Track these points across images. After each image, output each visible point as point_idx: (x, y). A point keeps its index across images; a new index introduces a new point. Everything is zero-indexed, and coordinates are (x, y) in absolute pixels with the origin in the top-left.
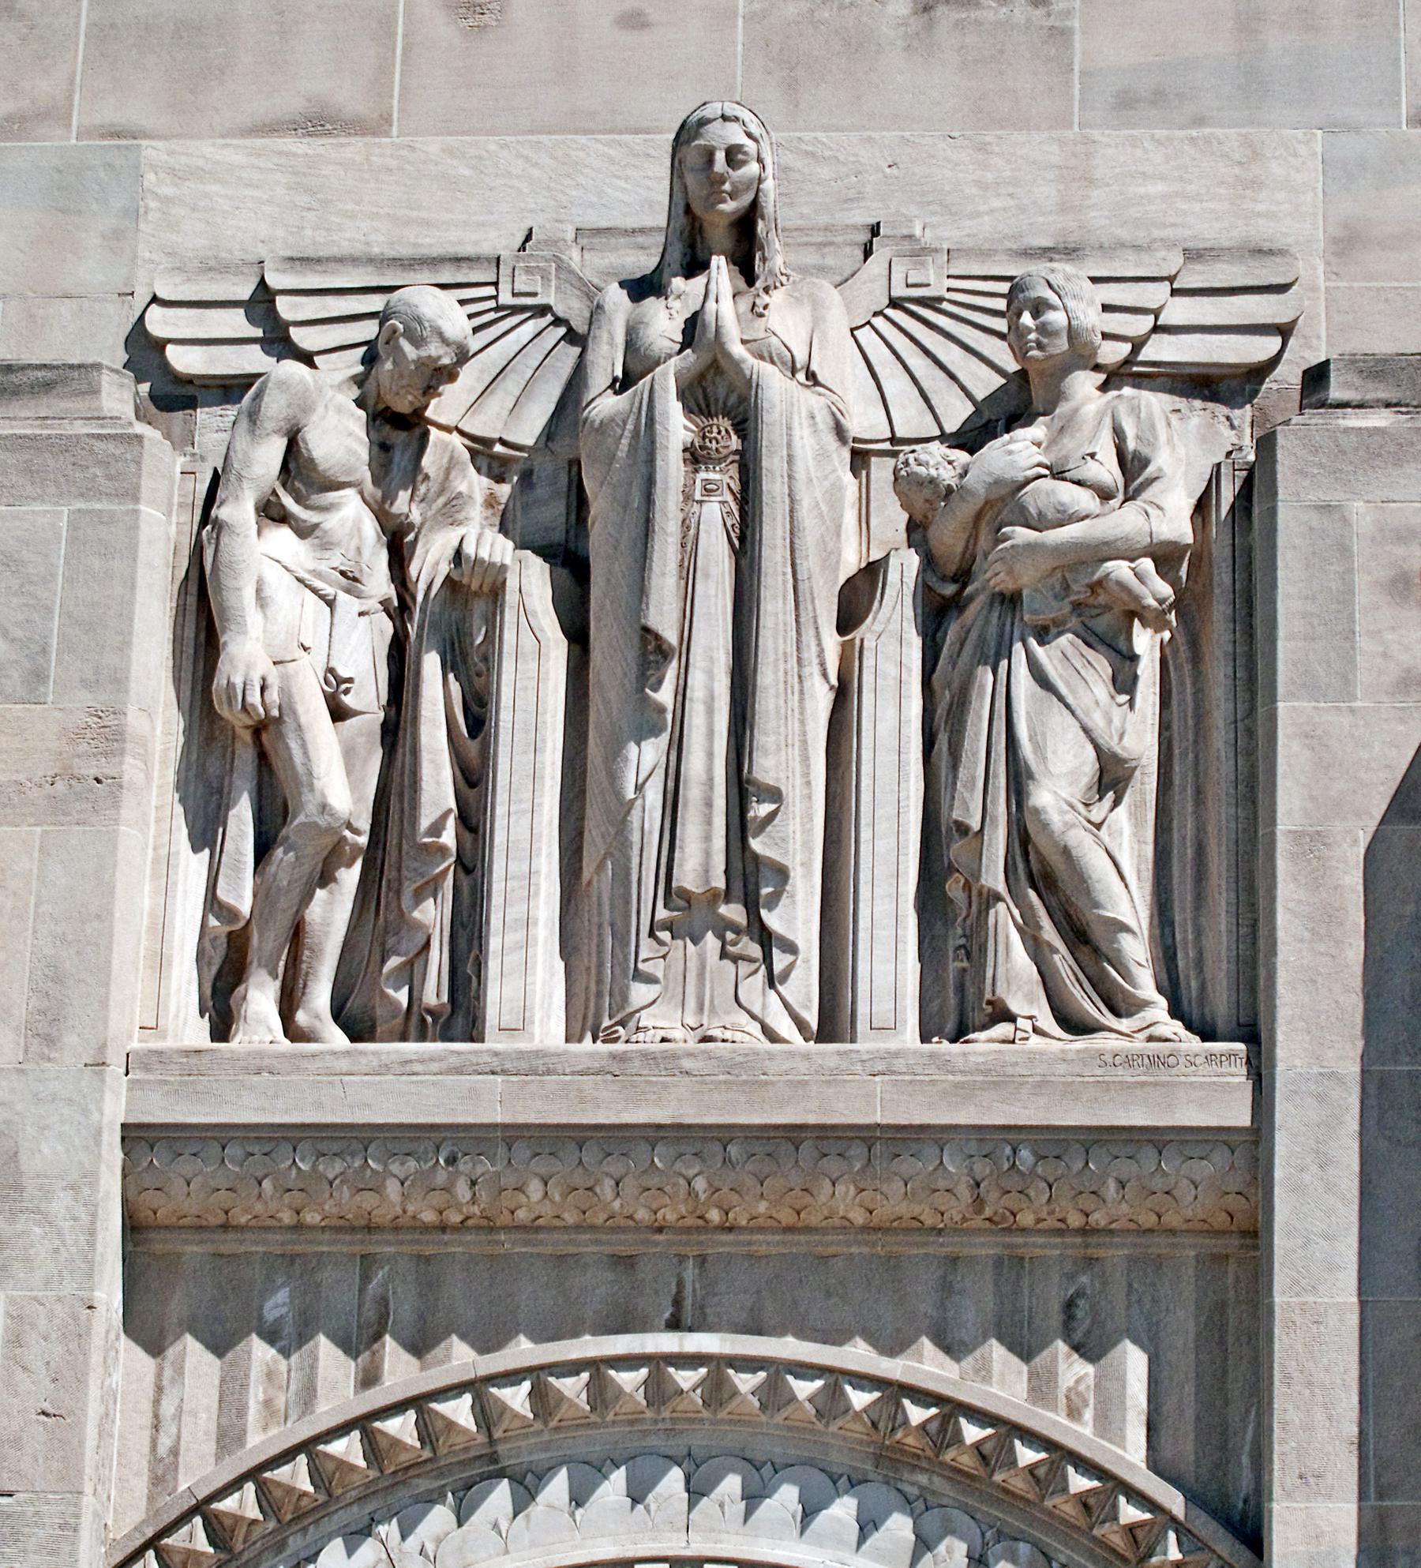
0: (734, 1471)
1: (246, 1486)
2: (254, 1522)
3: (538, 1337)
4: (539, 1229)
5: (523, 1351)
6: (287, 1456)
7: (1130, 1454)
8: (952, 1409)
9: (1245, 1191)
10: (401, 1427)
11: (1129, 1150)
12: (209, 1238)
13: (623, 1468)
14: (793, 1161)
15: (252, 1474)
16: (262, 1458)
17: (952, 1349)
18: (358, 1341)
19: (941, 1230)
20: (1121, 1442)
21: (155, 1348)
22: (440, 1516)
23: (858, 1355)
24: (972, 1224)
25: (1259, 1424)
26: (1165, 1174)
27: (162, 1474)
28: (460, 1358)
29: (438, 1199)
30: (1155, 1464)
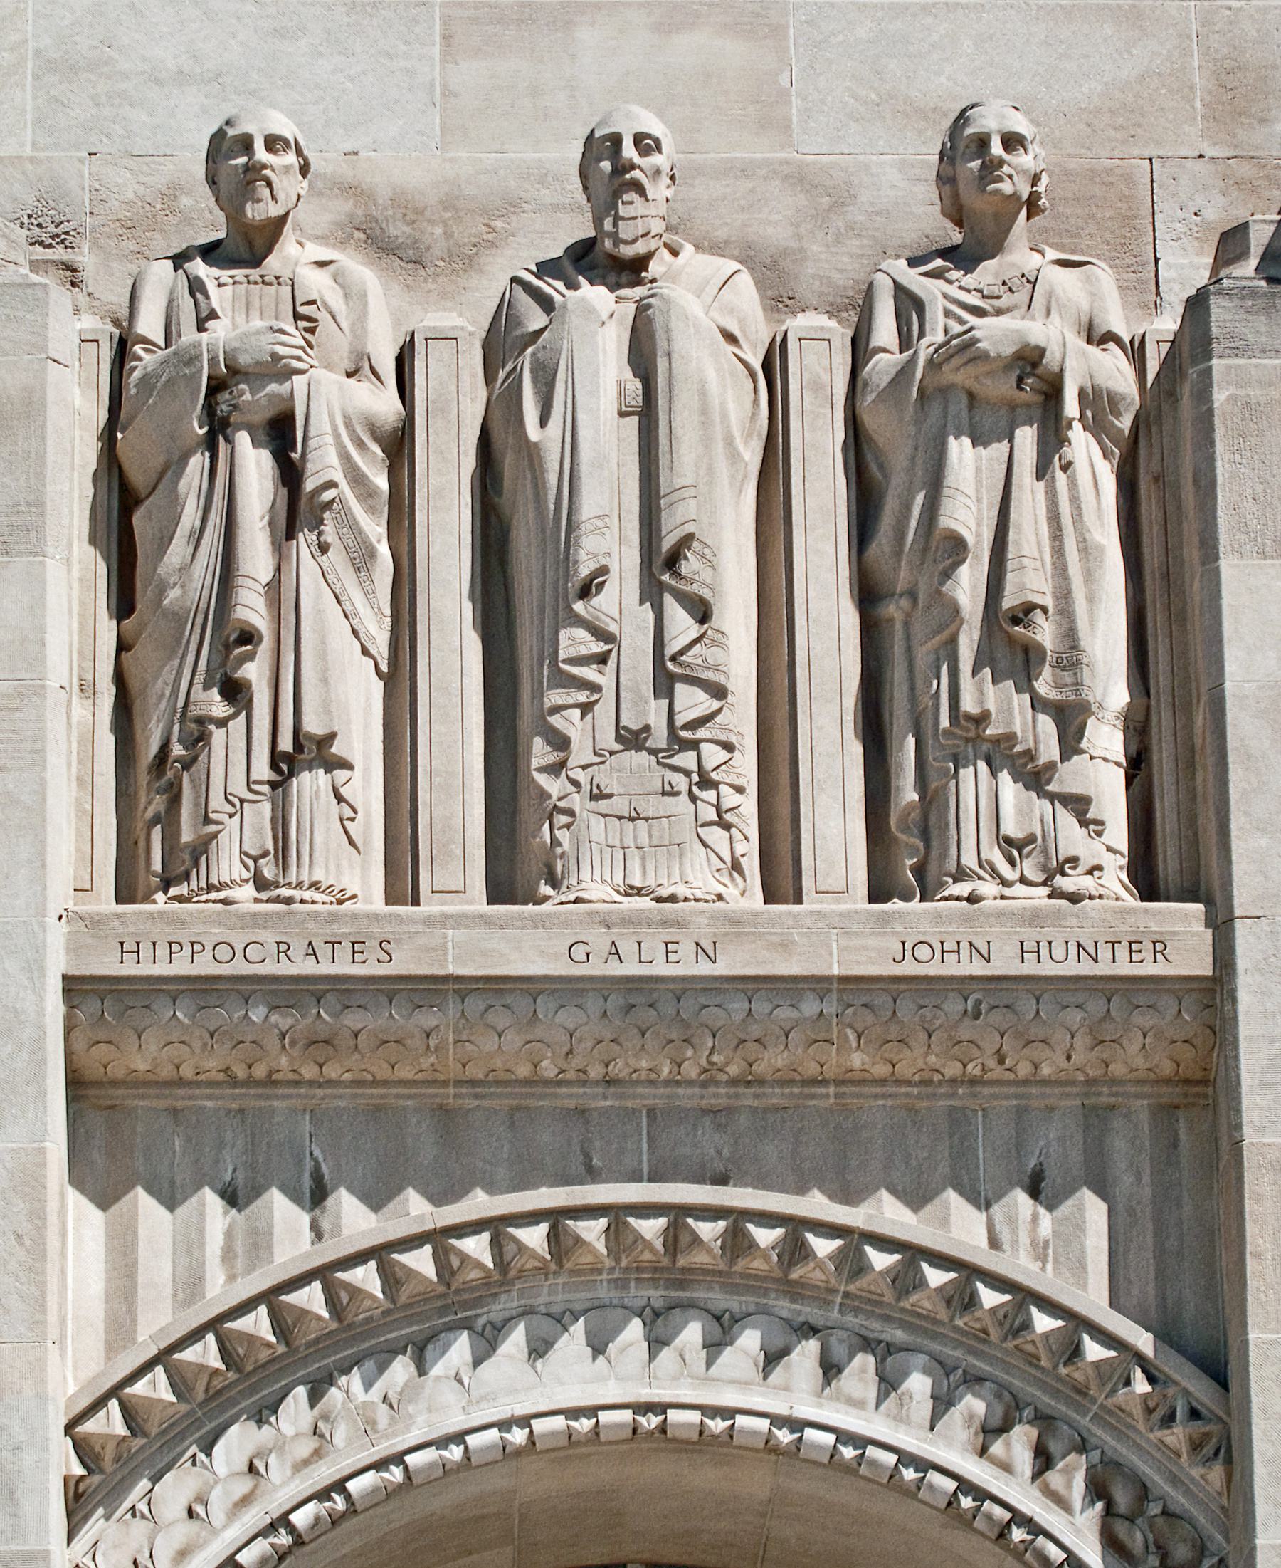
0: (694, 1319)
2: (217, 1371)
4: (275, 1083)
5: (480, 1203)
7: (1092, 1298)
8: (913, 1253)
12: (152, 1091)
13: (582, 1319)
15: (214, 1325)
17: (916, 1198)
18: (316, 1196)
19: (749, 1082)
20: (1084, 1286)
22: (401, 1369)
23: (816, 1205)
25: (535, 478)
27: (120, 1328)
28: (416, 1211)
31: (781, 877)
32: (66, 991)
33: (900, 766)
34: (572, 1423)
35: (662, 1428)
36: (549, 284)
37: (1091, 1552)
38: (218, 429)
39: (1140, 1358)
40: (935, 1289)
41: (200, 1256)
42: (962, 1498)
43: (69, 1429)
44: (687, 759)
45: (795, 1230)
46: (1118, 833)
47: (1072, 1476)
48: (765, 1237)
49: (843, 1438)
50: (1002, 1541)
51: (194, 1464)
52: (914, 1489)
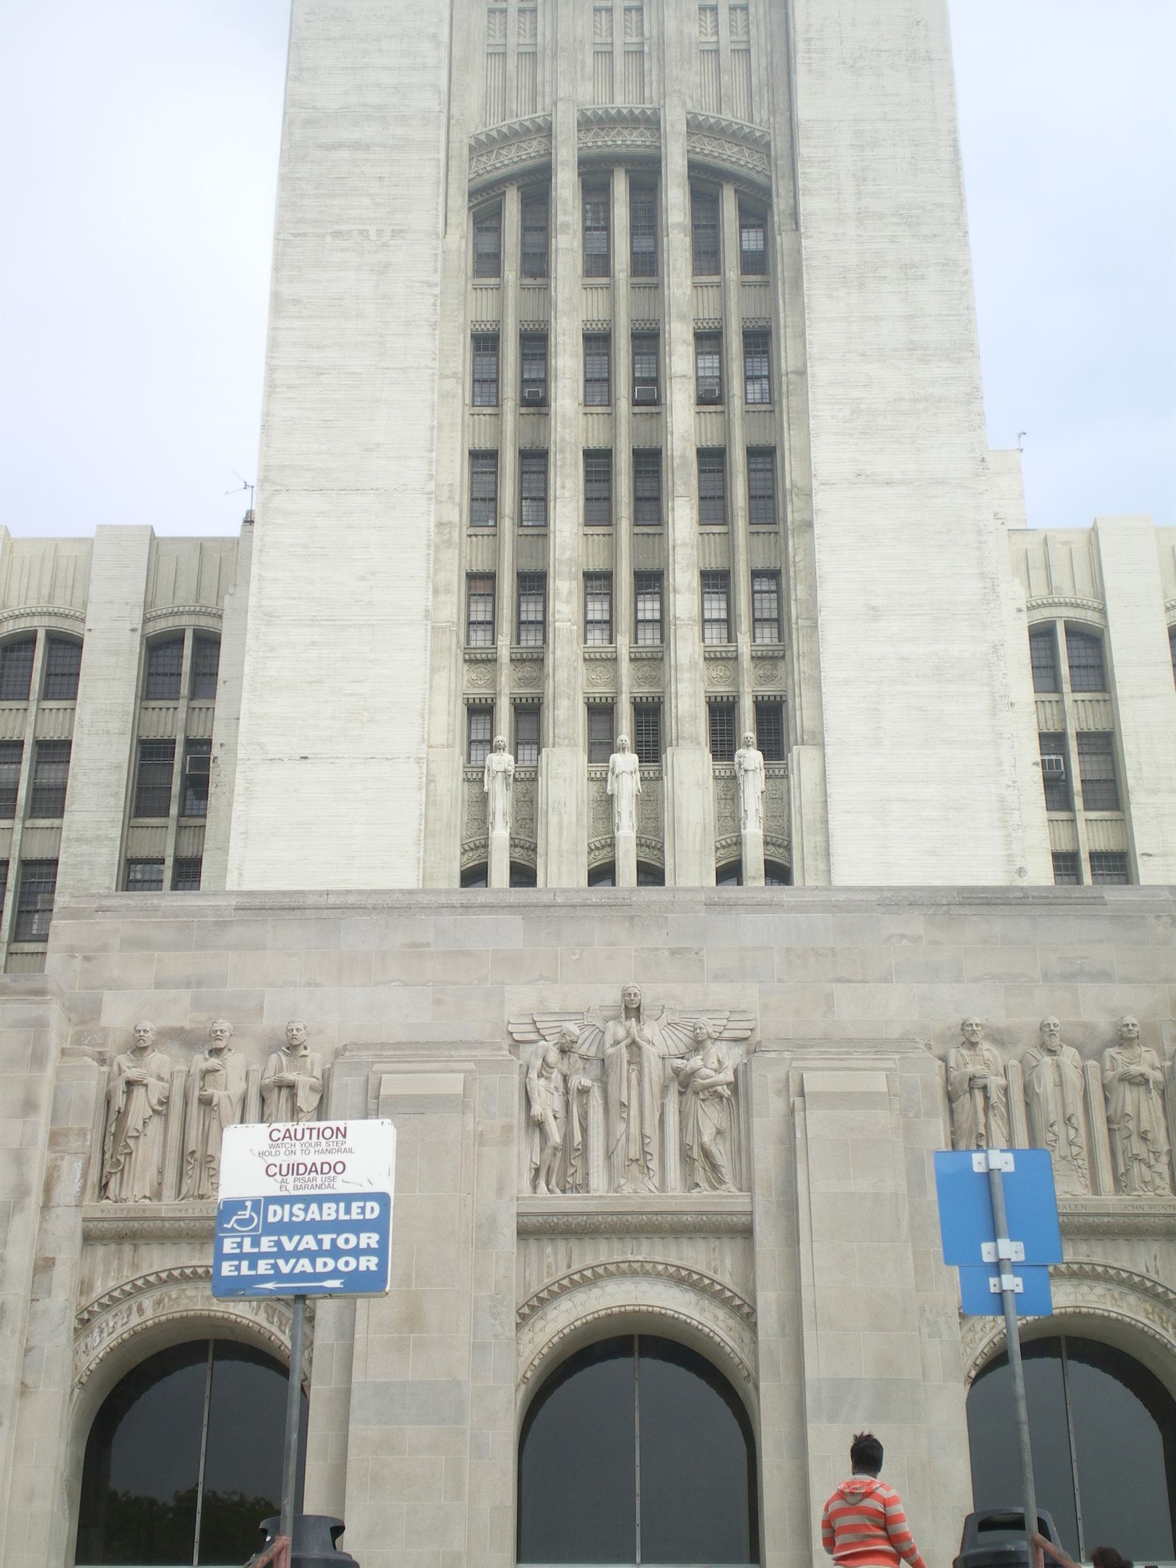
31: (1095, 1187)
32: (518, 1233)
33: (288, 1456)
38: (971, 1088)
44: (1075, 1163)
46: (1168, 1180)
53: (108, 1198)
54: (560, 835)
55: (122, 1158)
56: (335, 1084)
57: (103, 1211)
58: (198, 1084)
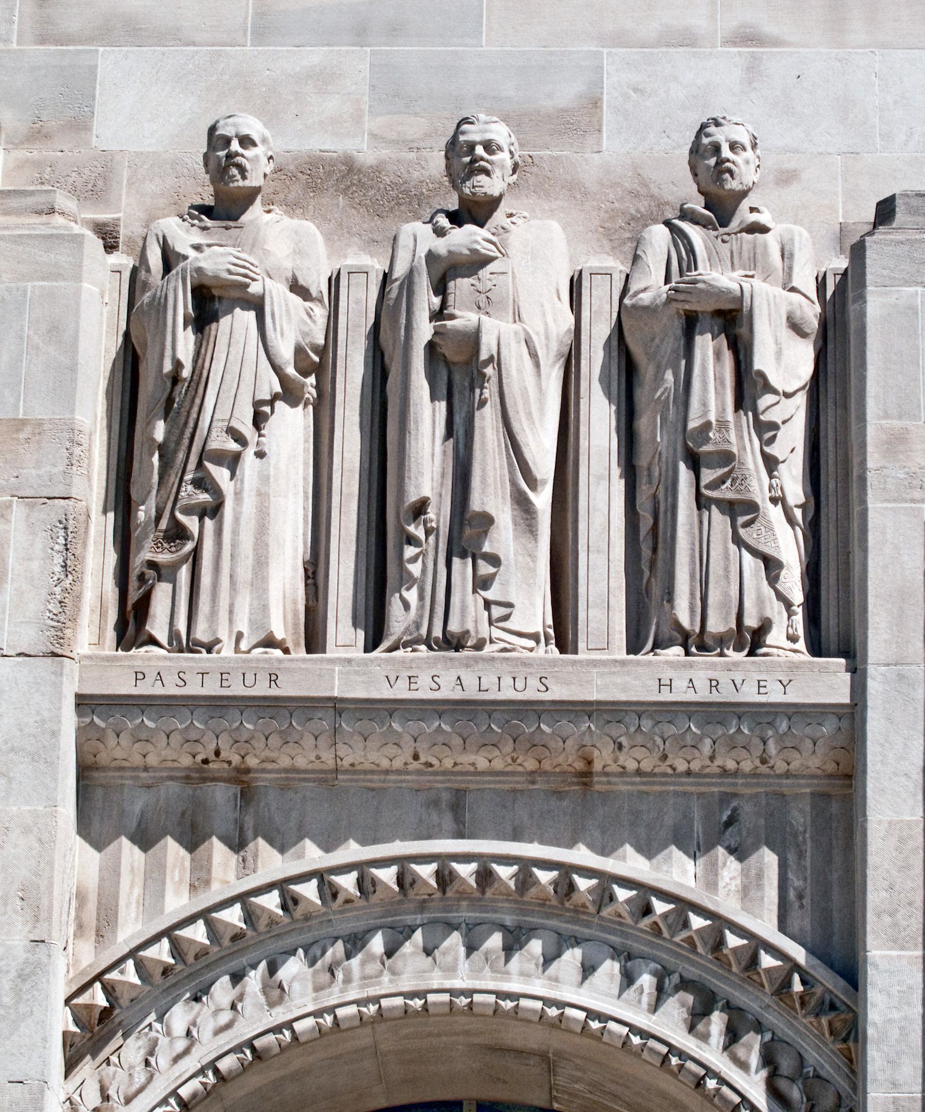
1: (163, 940)
3: (364, 842)
6: (190, 920)
7: (765, 925)
8: (645, 891)
9: (633, 744)
10: (271, 901)
11: (669, 717)
14: (289, 721)
15: (167, 933)
16: (175, 920)
21: (99, 845)
23: (581, 855)
24: (410, 767)
26: (794, 735)
28: (312, 855)
29: (688, 753)
30: (783, 927)
32: (78, 705)
34: (407, 1001)
35: (470, 1005)
36: (750, 440)
37: (758, 1095)
39: (796, 967)
40: (731, 949)
41: (166, 890)
42: (591, 1022)
43: (67, 1002)
45: (567, 873)
47: (752, 1047)
48: (545, 877)
49: (674, 1052)
50: (699, 1090)
51: (151, 1029)
52: (599, 1034)
53: (153, 641)
54: (740, 257)
55: (191, 523)
56: (877, 305)
57: (139, 676)
58: (426, 299)
